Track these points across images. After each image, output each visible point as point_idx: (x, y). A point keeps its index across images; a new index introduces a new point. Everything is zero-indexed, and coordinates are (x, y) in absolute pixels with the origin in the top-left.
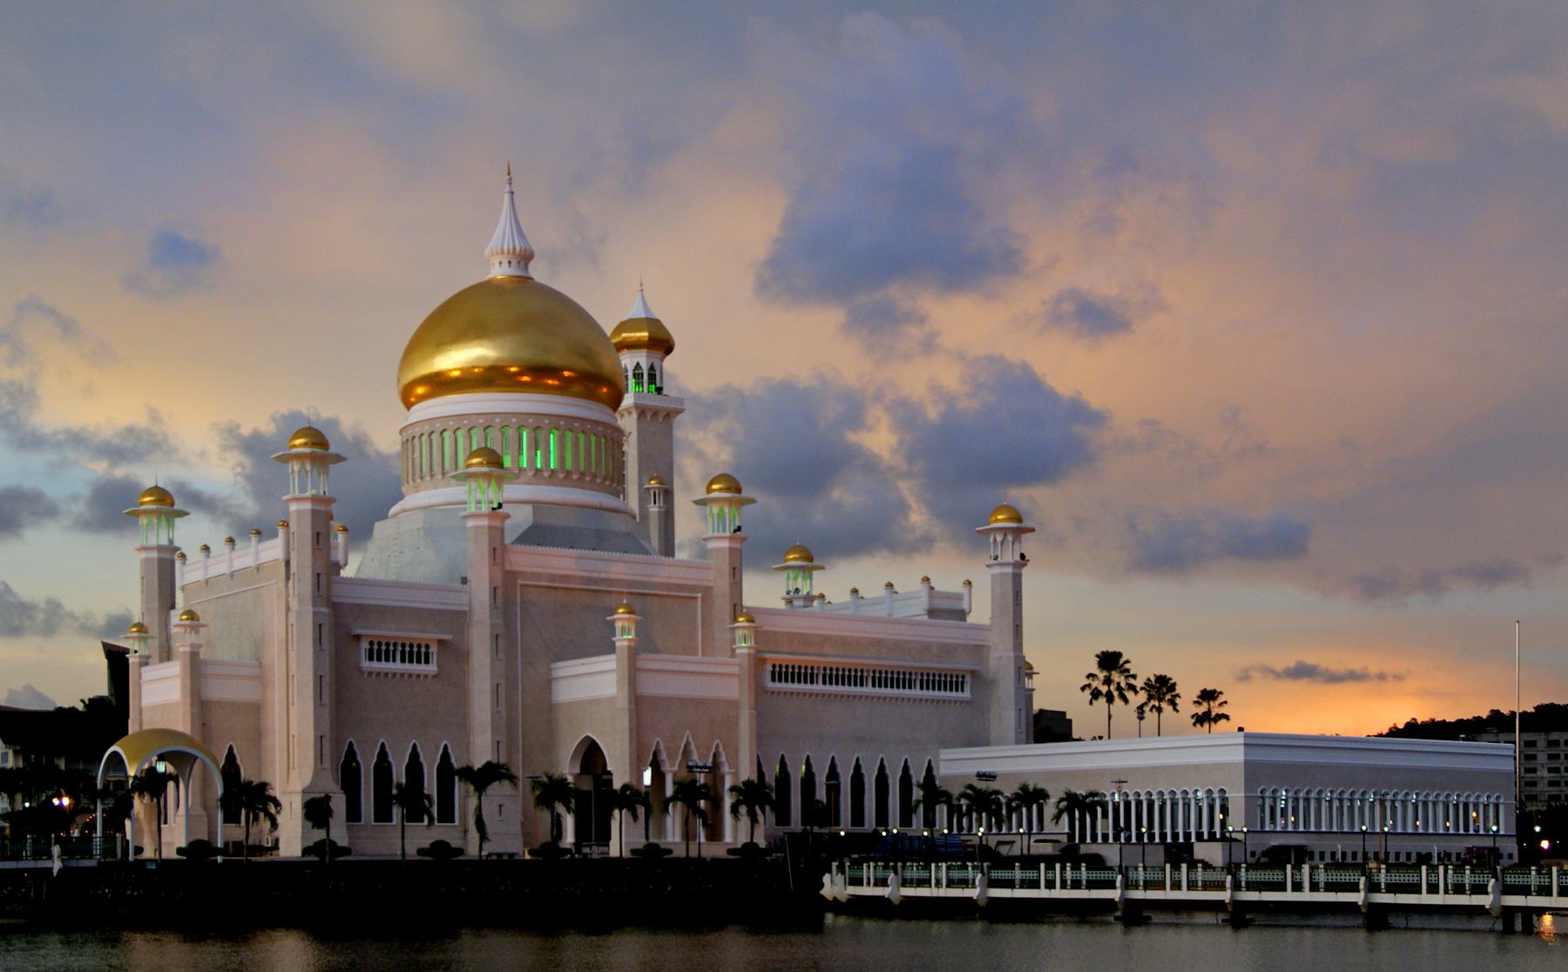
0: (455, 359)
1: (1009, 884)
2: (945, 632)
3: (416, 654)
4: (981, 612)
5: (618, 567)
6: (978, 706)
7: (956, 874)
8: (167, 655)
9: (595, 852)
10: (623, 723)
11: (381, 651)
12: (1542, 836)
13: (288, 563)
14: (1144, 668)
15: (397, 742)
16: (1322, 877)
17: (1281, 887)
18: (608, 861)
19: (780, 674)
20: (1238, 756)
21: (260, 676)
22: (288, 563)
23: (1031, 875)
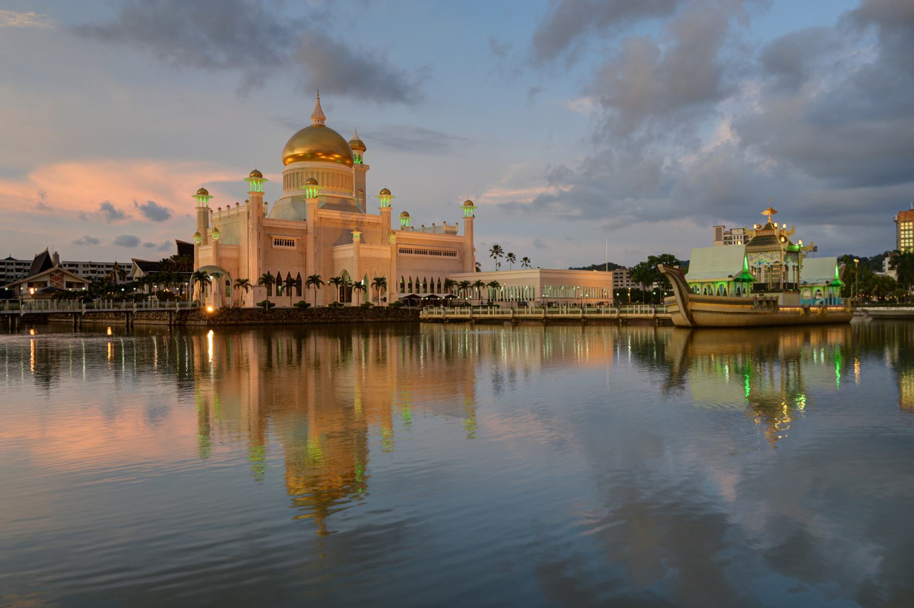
0: (299, 152)
1: (478, 313)
2: (450, 238)
3: (290, 243)
4: (461, 232)
5: (353, 217)
6: (462, 261)
7: (644, 309)
8: (206, 242)
9: (346, 304)
10: (356, 265)
11: (278, 243)
12: (784, 436)
13: (248, 214)
14: (506, 251)
15: (285, 269)
16: (569, 309)
17: (558, 312)
18: (353, 308)
19: (401, 251)
20: (538, 275)
21: (238, 249)
22: (248, 214)
23: (485, 310)
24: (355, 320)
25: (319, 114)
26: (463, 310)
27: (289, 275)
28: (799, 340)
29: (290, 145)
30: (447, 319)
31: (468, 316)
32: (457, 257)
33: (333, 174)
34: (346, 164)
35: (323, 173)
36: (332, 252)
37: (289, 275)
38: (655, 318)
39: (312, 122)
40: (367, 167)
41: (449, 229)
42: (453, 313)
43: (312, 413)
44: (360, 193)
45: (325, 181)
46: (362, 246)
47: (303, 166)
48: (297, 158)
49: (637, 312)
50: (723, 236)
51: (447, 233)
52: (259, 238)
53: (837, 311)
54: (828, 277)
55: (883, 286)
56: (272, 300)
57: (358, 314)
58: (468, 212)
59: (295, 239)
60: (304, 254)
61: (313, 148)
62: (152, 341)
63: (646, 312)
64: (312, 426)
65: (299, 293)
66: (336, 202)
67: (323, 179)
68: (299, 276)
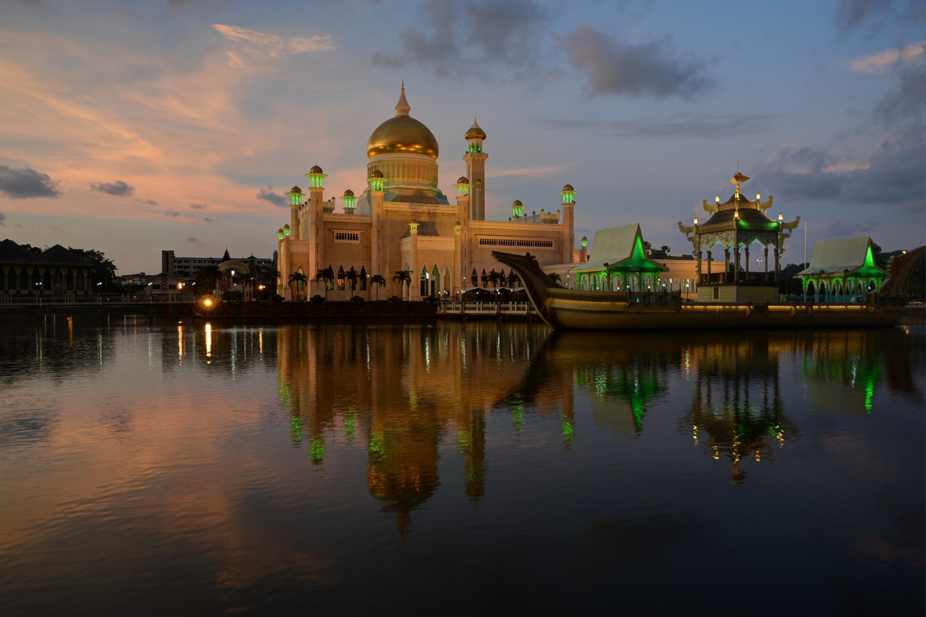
0: (380, 144)
3: (355, 237)
11: (339, 237)
25: (403, 104)
26: (486, 305)
27: (484, 272)
29: (374, 137)
32: (553, 248)
33: (398, 165)
35: (398, 165)
36: (400, 245)
37: (484, 272)
38: (529, 315)
39: (394, 114)
40: (487, 156)
41: (548, 217)
42: (475, 309)
43: (375, 410)
44: (478, 183)
46: (420, 238)
47: (381, 159)
48: (378, 150)
49: (513, 309)
51: (546, 221)
52: (317, 233)
54: (853, 263)
58: (568, 198)
59: (358, 233)
60: (368, 248)
61: (393, 139)
64: (375, 419)
65: (364, 288)
66: (410, 193)
67: (393, 171)
68: (363, 269)
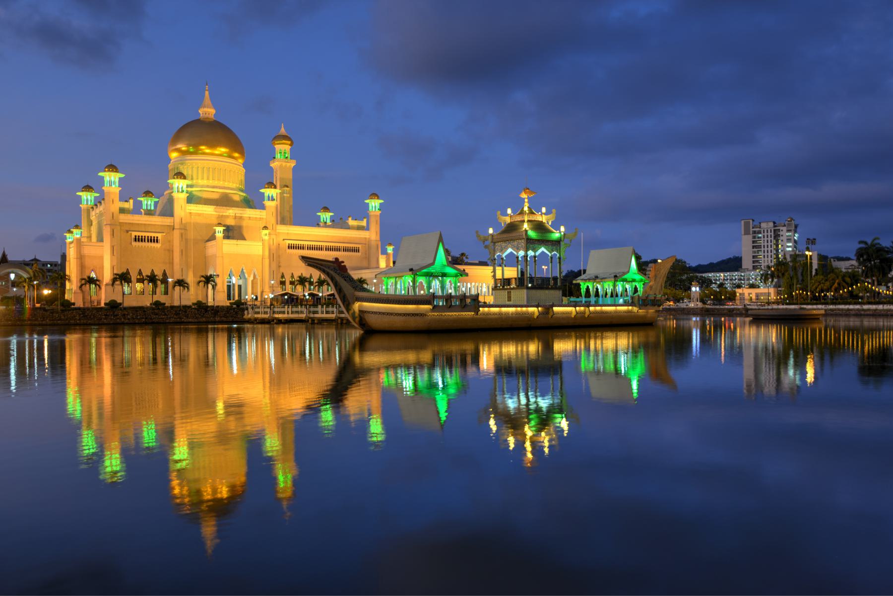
3: (156, 240)
11: (137, 239)
23: (315, 309)
24: (172, 320)
28: (580, 345)
30: (256, 319)
31: (303, 316)
34: (233, 158)
45: (205, 176)
50: (751, 230)
53: (795, 309)
55: (844, 281)
56: (163, 299)
57: (177, 314)
59: (160, 236)
62: (8, 343)
63: (297, 312)
